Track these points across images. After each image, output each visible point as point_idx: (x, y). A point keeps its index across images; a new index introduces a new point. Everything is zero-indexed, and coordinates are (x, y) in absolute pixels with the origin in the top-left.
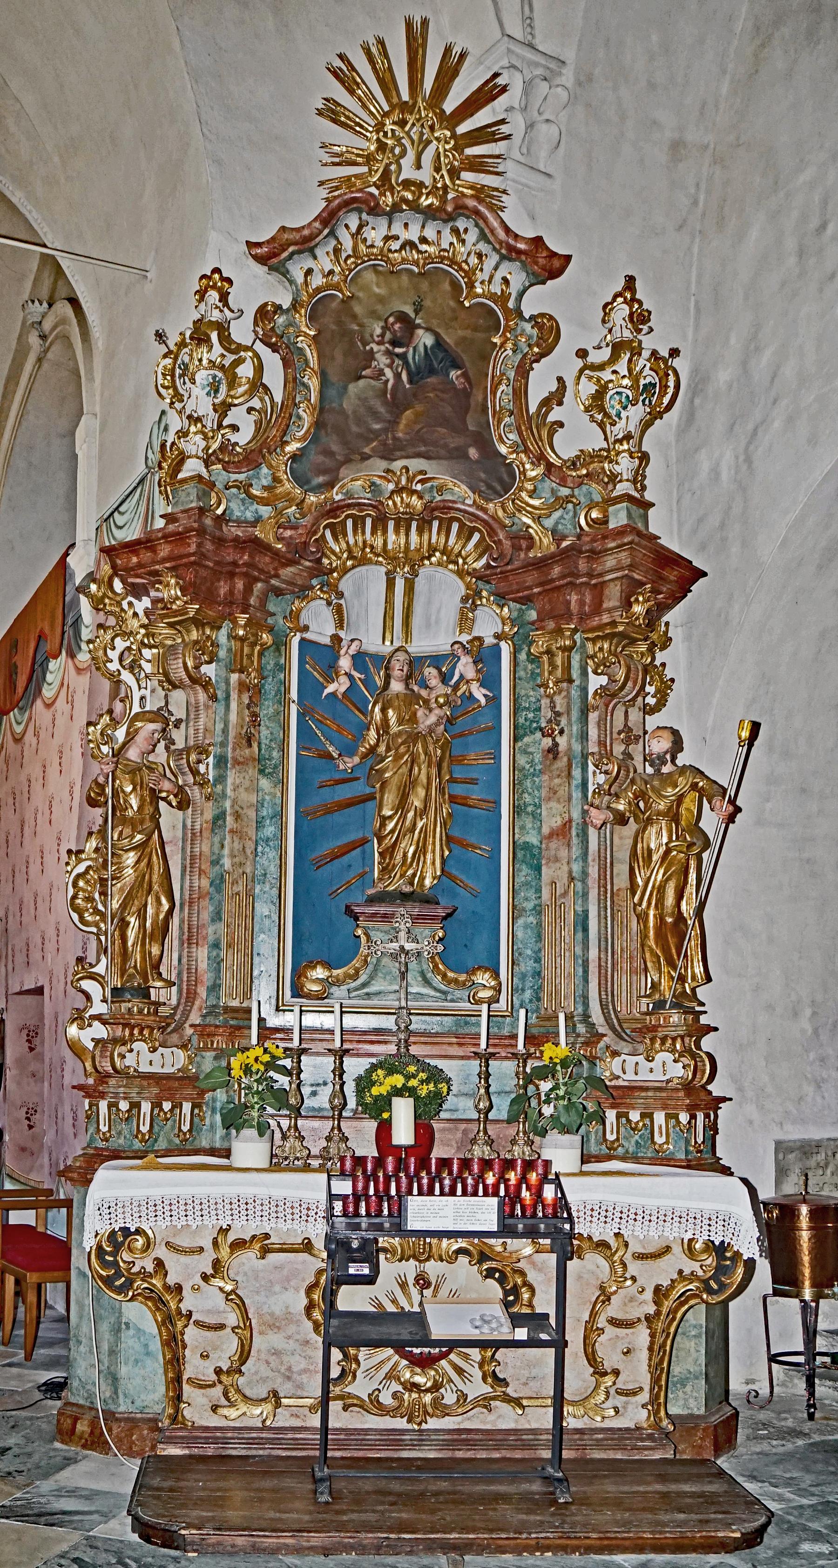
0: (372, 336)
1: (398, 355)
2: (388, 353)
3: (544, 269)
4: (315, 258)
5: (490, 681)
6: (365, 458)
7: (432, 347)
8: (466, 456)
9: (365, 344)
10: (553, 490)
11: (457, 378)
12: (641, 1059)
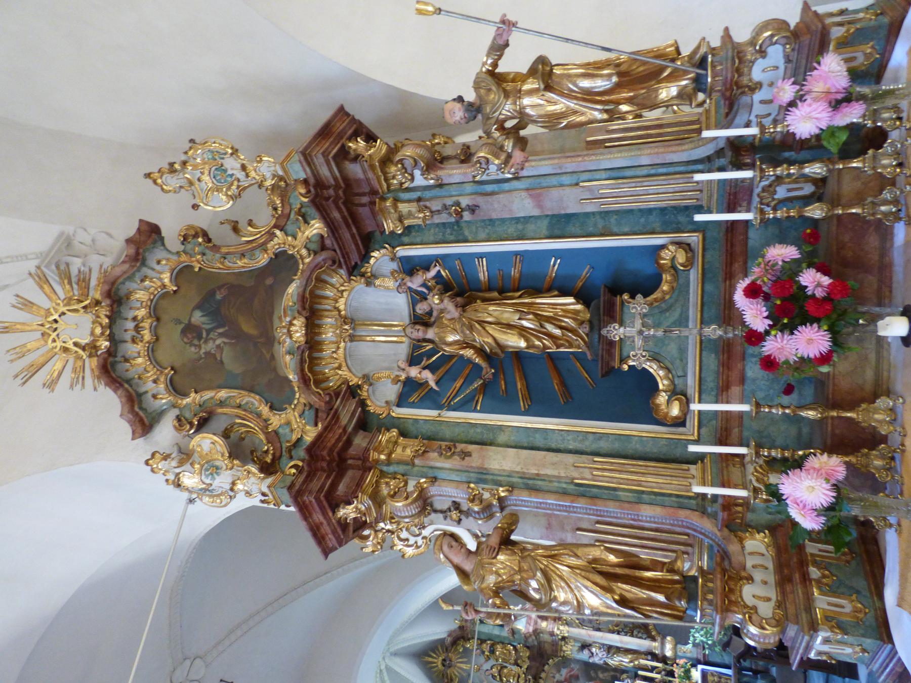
0: (196, 353)
1: (208, 335)
2: (206, 342)
3: (150, 236)
4: (146, 392)
5: (425, 264)
6: (273, 357)
7: (202, 311)
8: (271, 286)
9: (201, 358)
10: (292, 224)
11: (221, 294)
12: (758, 96)
